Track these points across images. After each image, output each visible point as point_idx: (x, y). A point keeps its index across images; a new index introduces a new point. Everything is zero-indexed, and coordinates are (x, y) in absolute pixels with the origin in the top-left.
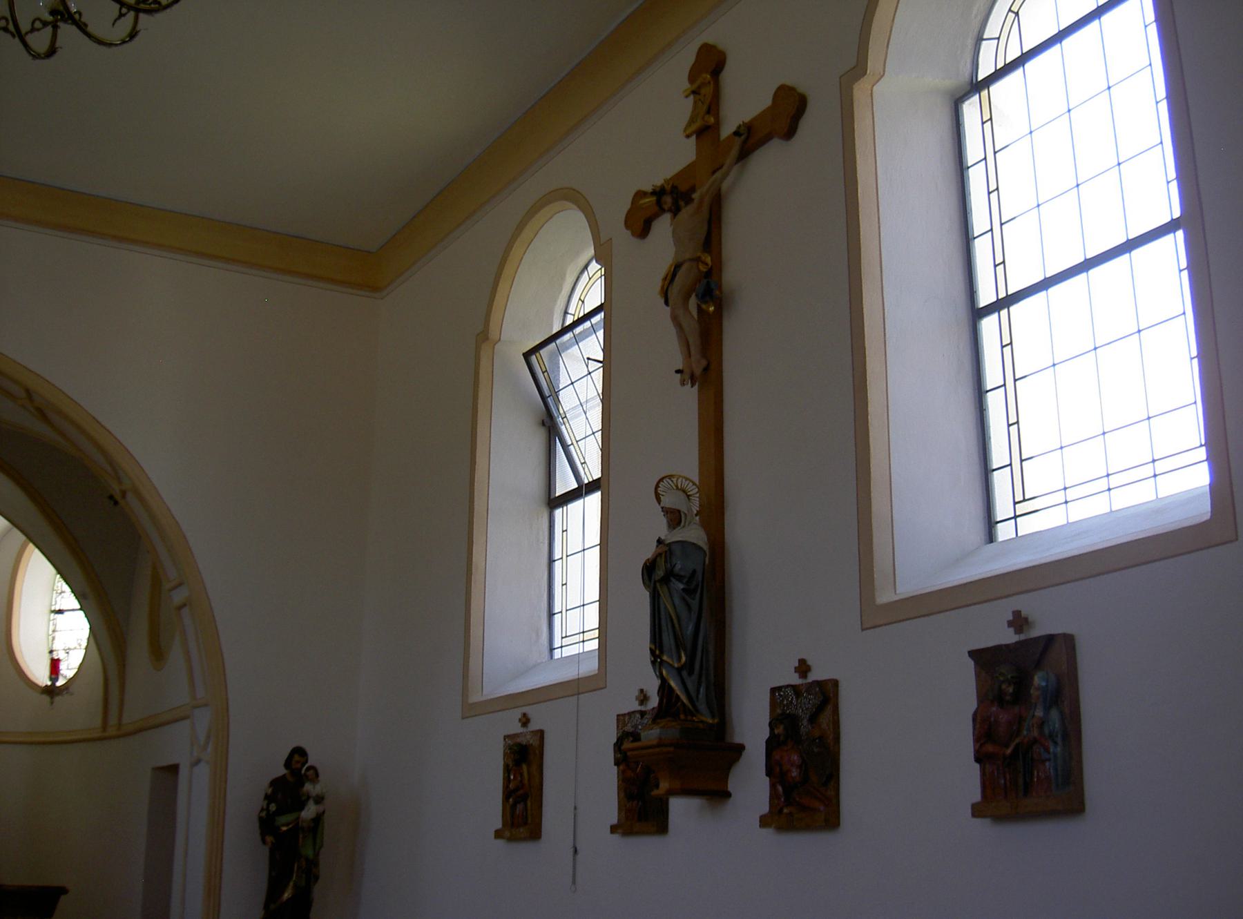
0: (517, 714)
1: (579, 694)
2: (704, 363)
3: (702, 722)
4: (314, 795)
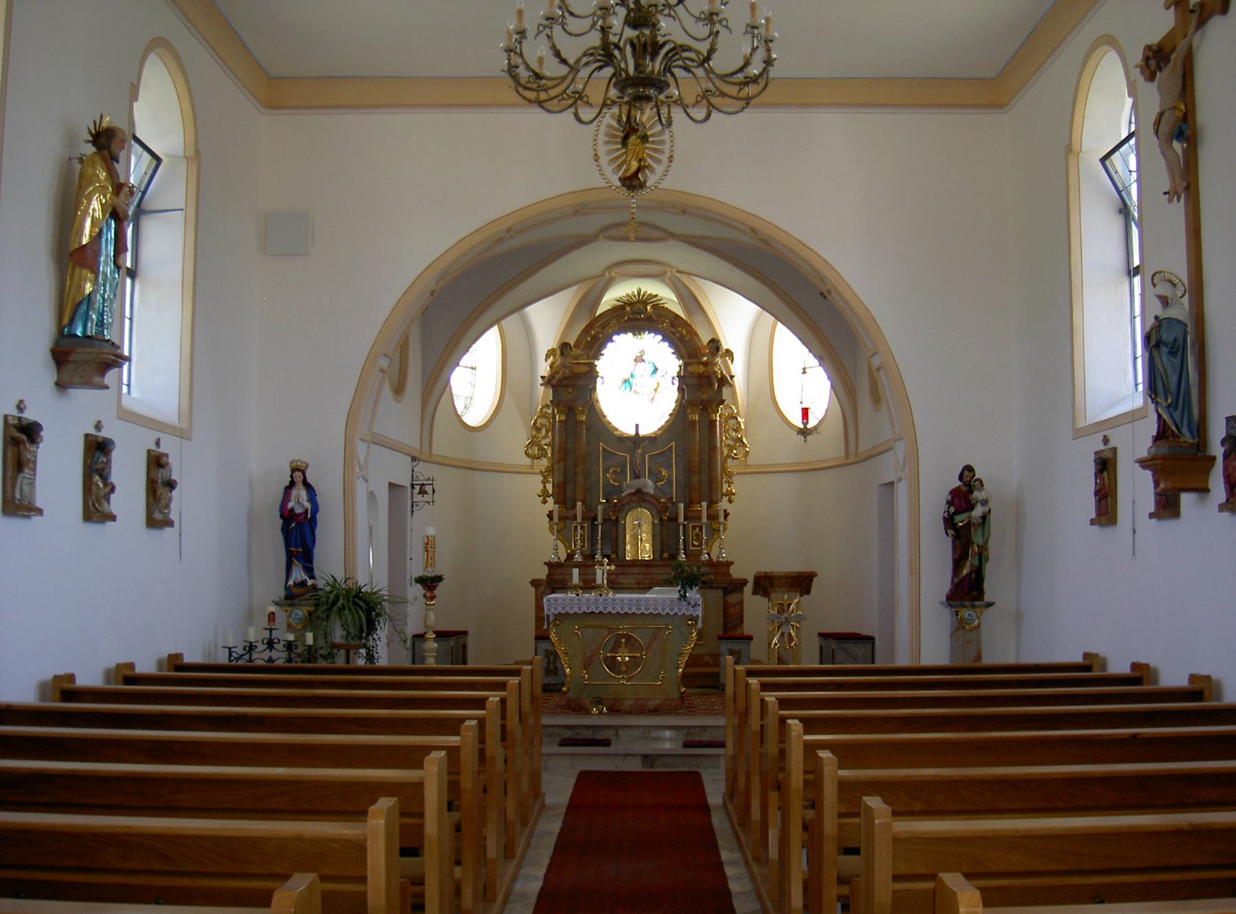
0: (1100, 436)
1: (1134, 421)
2: (1185, 184)
3: (1185, 442)
4: (981, 499)
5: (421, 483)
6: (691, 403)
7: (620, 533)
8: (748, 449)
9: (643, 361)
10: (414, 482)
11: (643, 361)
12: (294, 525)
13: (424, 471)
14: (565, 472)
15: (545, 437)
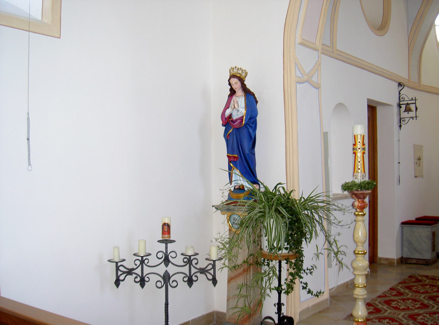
5: (406, 102)
10: (401, 103)
12: (231, 131)
13: (408, 94)
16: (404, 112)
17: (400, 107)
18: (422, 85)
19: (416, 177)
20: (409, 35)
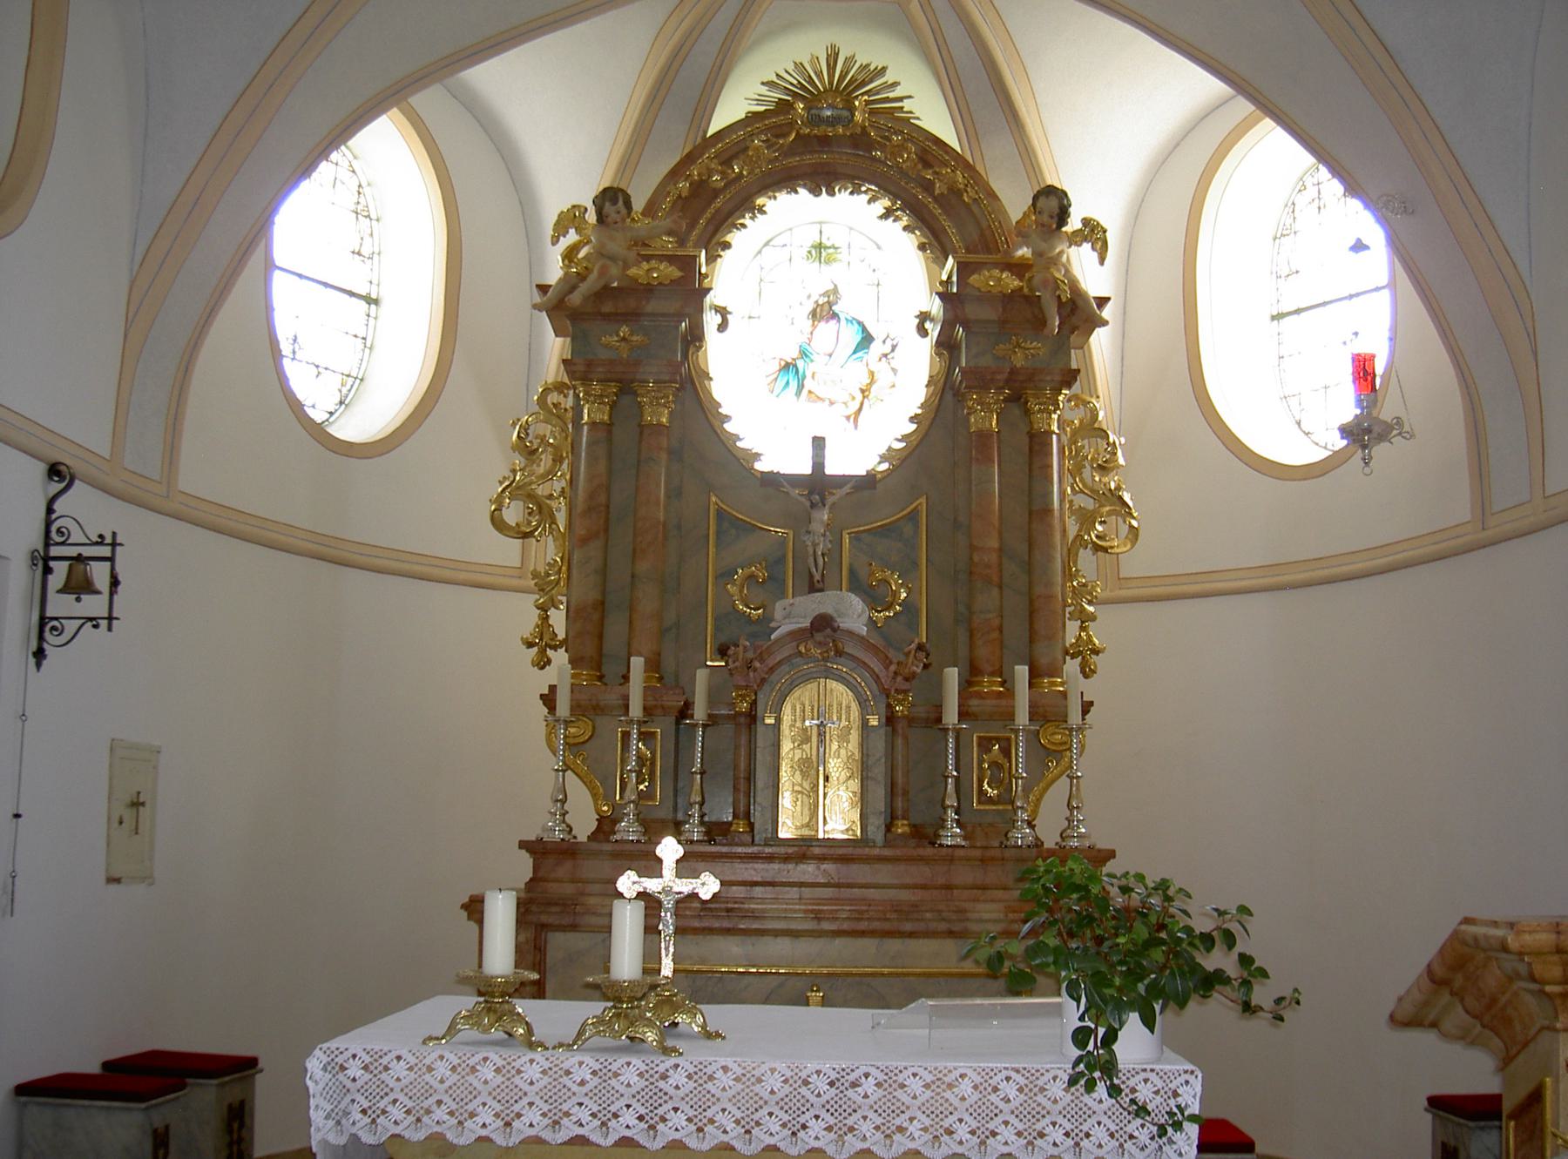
6: (979, 380)
7: (762, 757)
8: (1134, 523)
9: (835, 316)
10: (55, 551)
11: (835, 316)
14: (603, 572)
15: (549, 475)
16: (58, 592)
17: (47, 570)
18: (180, 492)
19: (113, 880)
20: (134, 273)
